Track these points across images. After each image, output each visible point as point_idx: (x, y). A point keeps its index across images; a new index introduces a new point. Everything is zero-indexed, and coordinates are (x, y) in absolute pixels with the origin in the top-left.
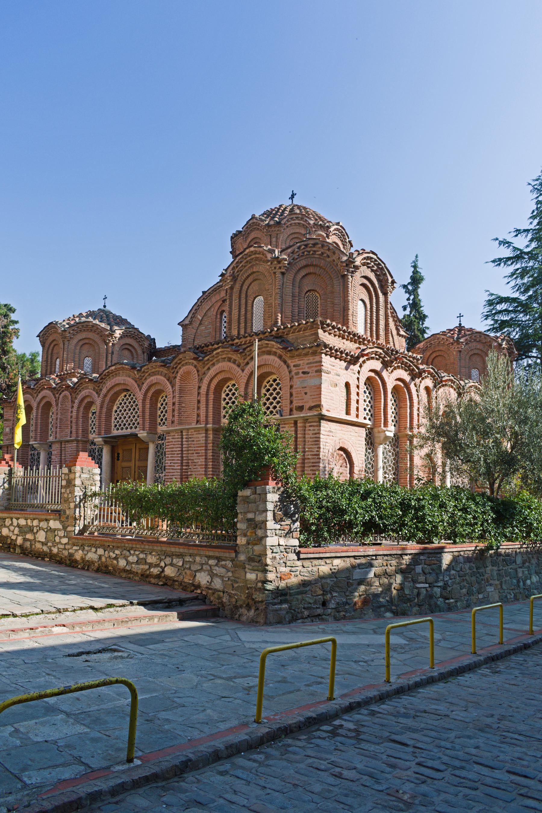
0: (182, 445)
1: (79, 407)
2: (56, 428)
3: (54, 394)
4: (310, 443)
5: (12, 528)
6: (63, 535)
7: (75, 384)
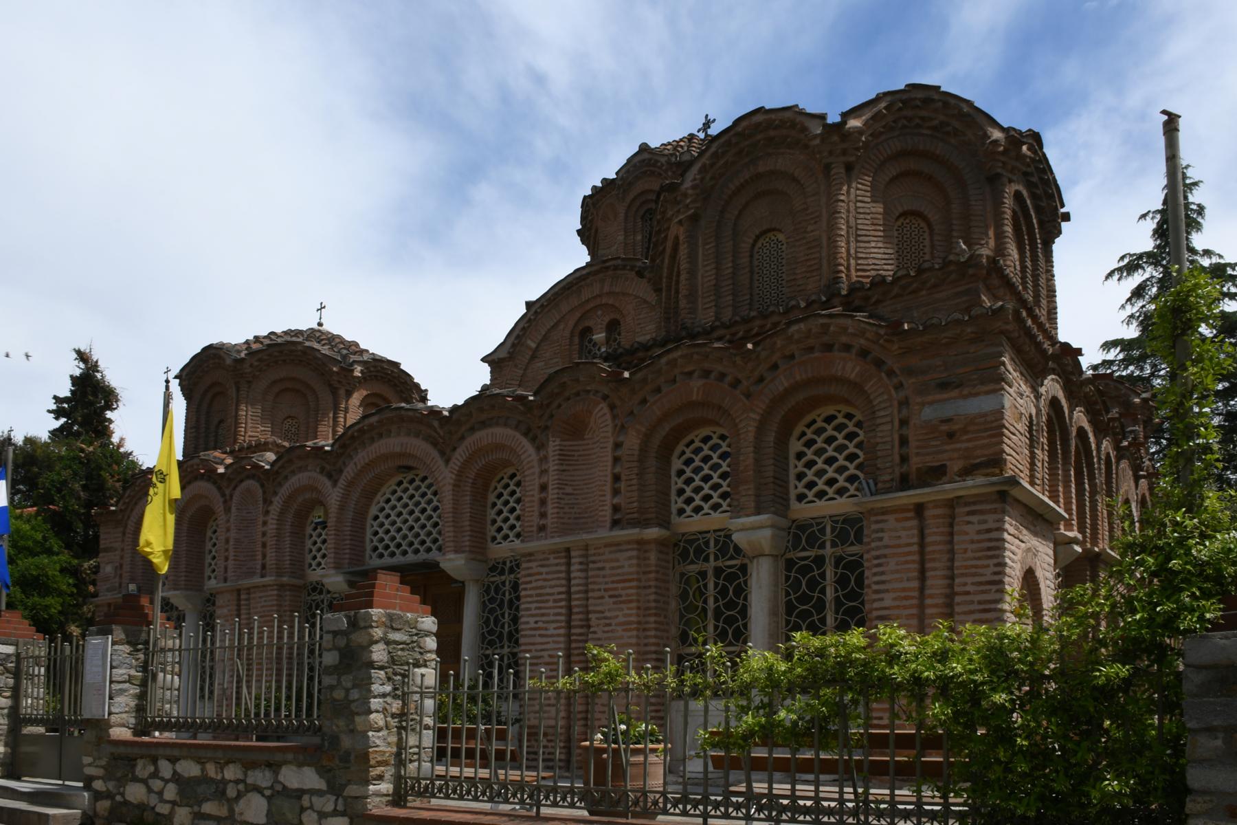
0: (569, 580)
1: (282, 513)
2: (227, 559)
3: (219, 488)
4: (970, 554)
5: (157, 784)
6: (329, 807)
7: (273, 464)
